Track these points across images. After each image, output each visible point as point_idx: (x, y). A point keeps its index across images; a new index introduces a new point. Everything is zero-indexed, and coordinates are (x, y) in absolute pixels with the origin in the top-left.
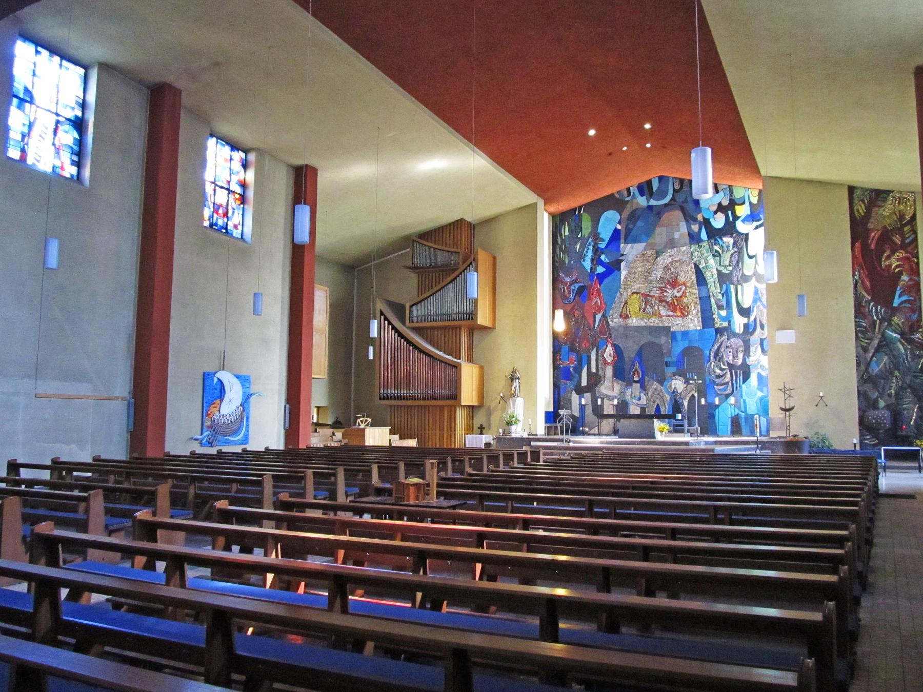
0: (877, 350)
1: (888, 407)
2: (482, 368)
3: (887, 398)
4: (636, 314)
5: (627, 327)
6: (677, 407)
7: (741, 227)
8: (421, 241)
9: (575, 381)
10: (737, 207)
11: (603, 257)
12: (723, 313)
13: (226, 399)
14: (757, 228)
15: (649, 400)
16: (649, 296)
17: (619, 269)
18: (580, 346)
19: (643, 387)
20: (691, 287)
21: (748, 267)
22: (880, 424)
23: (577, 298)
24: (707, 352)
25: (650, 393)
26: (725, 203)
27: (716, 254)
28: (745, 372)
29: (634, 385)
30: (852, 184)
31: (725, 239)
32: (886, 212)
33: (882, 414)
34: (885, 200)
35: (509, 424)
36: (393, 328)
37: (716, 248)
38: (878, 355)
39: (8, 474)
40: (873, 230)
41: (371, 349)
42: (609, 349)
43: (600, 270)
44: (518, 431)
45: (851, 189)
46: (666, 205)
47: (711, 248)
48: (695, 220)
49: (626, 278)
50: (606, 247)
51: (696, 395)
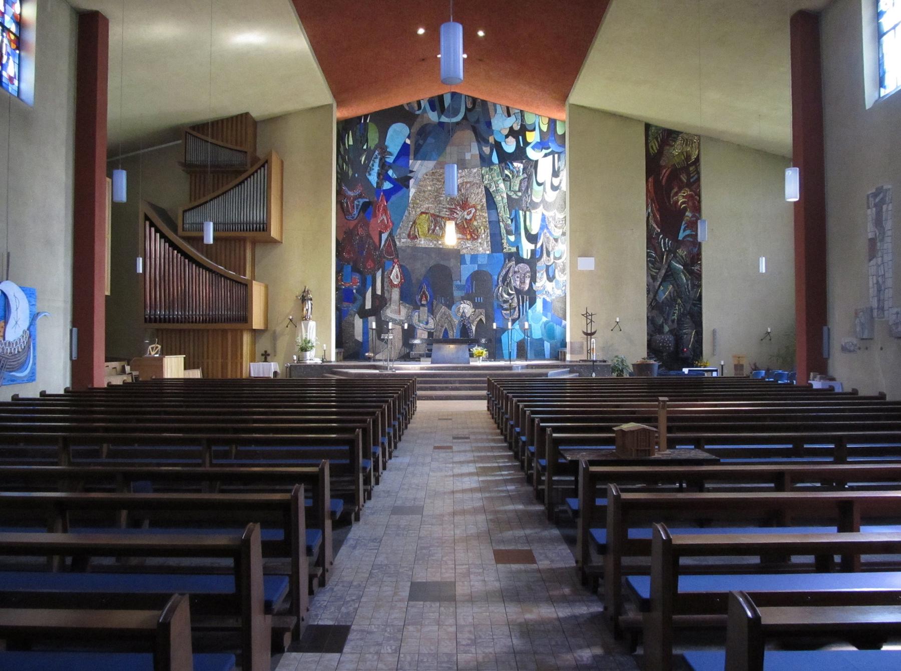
0: (664, 279)
1: (671, 331)
2: (267, 287)
3: (670, 323)
4: (425, 236)
5: (415, 249)
6: (465, 330)
7: (531, 153)
8: (195, 133)
9: (358, 303)
10: (527, 133)
11: (390, 172)
12: (512, 238)
13: (12, 321)
14: (546, 155)
15: (436, 324)
16: (438, 216)
17: (408, 187)
18: (365, 267)
19: (432, 311)
20: (481, 210)
21: (537, 194)
22: (665, 347)
23: (362, 214)
24: (496, 277)
25: (438, 316)
26: (517, 127)
27: (506, 179)
28: (531, 296)
29: (421, 308)
30: (648, 121)
31: (515, 164)
32: (676, 150)
33: (666, 338)
34: (675, 140)
35: (304, 349)
36: (163, 236)
37: (507, 172)
38: (664, 284)
39: (604, 526)
40: (665, 167)
41: (140, 261)
42: (396, 270)
43: (387, 185)
44: (312, 358)
45: (648, 126)
46: (457, 123)
47: (502, 172)
48: (486, 142)
49: (414, 196)
50: (394, 161)
51: (484, 320)
